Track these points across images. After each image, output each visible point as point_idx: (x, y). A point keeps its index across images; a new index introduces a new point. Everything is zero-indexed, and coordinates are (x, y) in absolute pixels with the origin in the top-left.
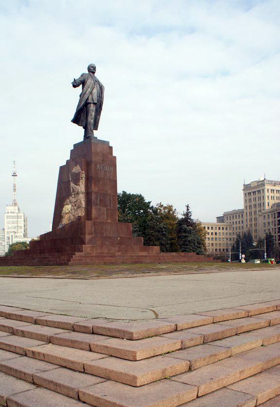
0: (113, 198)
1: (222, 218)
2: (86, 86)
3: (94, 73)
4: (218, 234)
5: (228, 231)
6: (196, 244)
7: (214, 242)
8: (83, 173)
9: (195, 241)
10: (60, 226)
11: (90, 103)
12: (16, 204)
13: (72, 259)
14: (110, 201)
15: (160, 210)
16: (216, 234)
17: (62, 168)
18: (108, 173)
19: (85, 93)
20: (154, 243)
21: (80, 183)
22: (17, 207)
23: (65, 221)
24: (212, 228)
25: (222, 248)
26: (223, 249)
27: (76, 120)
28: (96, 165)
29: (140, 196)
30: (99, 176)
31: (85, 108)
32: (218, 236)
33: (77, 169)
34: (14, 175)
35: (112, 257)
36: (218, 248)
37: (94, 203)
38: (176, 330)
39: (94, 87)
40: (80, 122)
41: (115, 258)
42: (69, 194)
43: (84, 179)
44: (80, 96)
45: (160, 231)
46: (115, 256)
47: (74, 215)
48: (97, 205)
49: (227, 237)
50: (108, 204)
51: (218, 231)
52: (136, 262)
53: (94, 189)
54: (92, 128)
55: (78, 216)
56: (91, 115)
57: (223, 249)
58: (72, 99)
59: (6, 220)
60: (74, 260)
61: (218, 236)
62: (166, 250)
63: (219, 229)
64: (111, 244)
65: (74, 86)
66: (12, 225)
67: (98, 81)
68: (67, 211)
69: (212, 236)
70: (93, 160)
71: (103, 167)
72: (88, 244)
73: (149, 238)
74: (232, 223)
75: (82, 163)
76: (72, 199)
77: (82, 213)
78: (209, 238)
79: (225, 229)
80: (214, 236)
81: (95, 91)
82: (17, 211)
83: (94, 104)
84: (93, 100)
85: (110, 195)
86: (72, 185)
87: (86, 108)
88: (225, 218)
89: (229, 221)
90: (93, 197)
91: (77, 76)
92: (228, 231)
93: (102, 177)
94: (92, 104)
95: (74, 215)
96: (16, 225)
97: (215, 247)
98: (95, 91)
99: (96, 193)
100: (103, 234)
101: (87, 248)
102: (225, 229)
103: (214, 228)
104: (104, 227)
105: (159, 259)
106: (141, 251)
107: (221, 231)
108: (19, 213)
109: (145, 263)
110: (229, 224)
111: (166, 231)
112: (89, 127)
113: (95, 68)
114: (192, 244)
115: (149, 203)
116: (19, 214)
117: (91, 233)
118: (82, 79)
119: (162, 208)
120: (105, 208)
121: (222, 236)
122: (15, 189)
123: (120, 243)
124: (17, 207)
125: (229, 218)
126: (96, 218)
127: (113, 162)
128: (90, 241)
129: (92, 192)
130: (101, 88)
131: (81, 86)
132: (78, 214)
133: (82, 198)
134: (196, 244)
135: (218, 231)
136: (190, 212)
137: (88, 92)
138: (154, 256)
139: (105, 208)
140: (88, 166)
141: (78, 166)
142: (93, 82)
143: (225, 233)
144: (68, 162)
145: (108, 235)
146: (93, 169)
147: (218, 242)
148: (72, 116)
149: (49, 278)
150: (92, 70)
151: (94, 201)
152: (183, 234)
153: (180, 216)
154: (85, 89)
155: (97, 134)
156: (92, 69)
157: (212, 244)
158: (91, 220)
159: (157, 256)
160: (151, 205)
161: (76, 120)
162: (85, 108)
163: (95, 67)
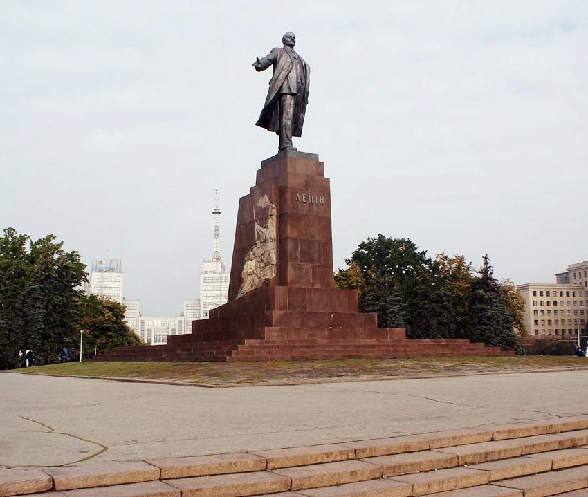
0: (324, 249)
1: (565, 275)
2: (278, 68)
3: (292, 46)
4: (558, 303)
5: (578, 298)
6: (501, 323)
7: (552, 318)
8: (273, 208)
9: (498, 317)
10: (239, 296)
11: (286, 94)
12: (218, 259)
13: (234, 351)
14: (320, 251)
15: (444, 264)
16: (555, 303)
17: (242, 200)
18: (315, 207)
19: (277, 79)
20: (427, 322)
21: (269, 224)
22: (219, 264)
23: (247, 287)
24: (541, 294)
25: (567, 328)
26: (563, 330)
27: (265, 122)
28: (294, 194)
29: (409, 242)
30: (299, 212)
31: (278, 102)
32: (558, 307)
33: (264, 201)
34: (217, 212)
35: (308, 347)
36: (560, 328)
37: (290, 257)
38: (53, 489)
39: (292, 68)
40: (271, 126)
41: (314, 349)
42: (252, 244)
43: (274, 217)
44: (270, 84)
45: (438, 300)
46: (314, 347)
47: (259, 278)
48: (296, 258)
49: (576, 308)
50: (316, 258)
51: (558, 298)
52: (350, 357)
53: (291, 232)
54: (289, 133)
55: (266, 279)
56: (287, 113)
57: (570, 331)
58: (258, 90)
59: (202, 284)
60: (238, 353)
61: (558, 307)
62: (450, 333)
63: (561, 294)
64: (318, 325)
65: (258, 69)
66: (211, 292)
67: (299, 57)
68: (249, 271)
69: (549, 308)
70: (289, 186)
71: (307, 197)
72: (276, 325)
73: (420, 313)
74: (583, 284)
75: (271, 191)
76: (257, 250)
77: (271, 274)
78: (542, 311)
79: (571, 294)
80: (552, 307)
81: (293, 75)
82: (220, 270)
83: (292, 94)
84: (289, 88)
85: (320, 244)
86: (257, 227)
87: (280, 101)
88: (571, 276)
89: (578, 280)
90: (290, 246)
91: (264, 54)
92: (578, 298)
93: (305, 212)
94: (288, 96)
95: (259, 278)
96: (219, 292)
97: (554, 327)
98: (293, 75)
99: (295, 240)
100: (305, 308)
101: (272, 333)
102: (571, 294)
103: (551, 293)
104: (307, 298)
105: (396, 351)
106: (371, 337)
107: (565, 298)
108: (222, 273)
109: (368, 358)
110: (578, 285)
111: (448, 301)
112: (284, 133)
113: (293, 39)
114: (495, 323)
115: (424, 253)
116: (223, 275)
117: (283, 308)
118: (271, 58)
119: (446, 262)
120: (311, 266)
121: (566, 307)
122: (218, 235)
123: (335, 323)
124: (219, 264)
125: (577, 275)
126: (293, 282)
127: (324, 189)
128: (280, 322)
129: (286, 238)
130: (305, 70)
131: (271, 67)
132: (266, 275)
133: (272, 248)
134: (501, 323)
135: (558, 298)
136: (490, 267)
137: (281, 77)
138: (388, 346)
139: (311, 266)
140: (281, 195)
141: (266, 196)
142: (289, 60)
143: (572, 302)
144: (252, 190)
145: (315, 311)
146: (289, 201)
147: (559, 317)
148: (257, 117)
149: (164, 383)
150: (289, 42)
151: (291, 253)
152: (478, 306)
153: (476, 275)
154: (276, 72)
155: (299, 144)
156: (289, 39)
157: (549, 321)
158: (286, 285)
159: (393, 346)
160: (427, 257)
161: (265, 122)
162: (278, 102)
163: (294, 37)
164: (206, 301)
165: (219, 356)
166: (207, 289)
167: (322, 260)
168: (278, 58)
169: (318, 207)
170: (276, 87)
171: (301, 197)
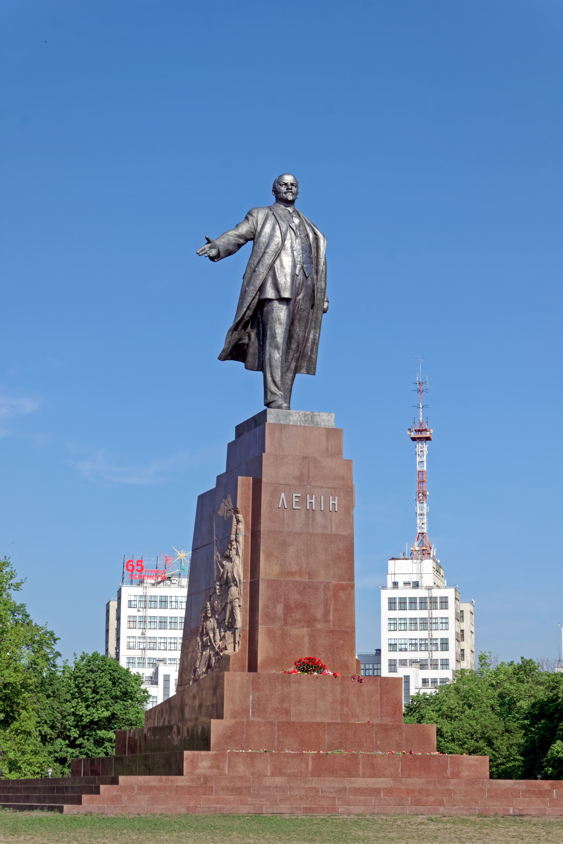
11: (270, 300)
18: (319, 519)
56: (274, 336)
59: (386, 614)
71: (303, 500)
164: (398, 656)
165: (302, 806)
166: (394, 624)
167: (331, 618)
168: (259, 229)
169: (324, 516)
170: (252, 288)
171: (290, 501)
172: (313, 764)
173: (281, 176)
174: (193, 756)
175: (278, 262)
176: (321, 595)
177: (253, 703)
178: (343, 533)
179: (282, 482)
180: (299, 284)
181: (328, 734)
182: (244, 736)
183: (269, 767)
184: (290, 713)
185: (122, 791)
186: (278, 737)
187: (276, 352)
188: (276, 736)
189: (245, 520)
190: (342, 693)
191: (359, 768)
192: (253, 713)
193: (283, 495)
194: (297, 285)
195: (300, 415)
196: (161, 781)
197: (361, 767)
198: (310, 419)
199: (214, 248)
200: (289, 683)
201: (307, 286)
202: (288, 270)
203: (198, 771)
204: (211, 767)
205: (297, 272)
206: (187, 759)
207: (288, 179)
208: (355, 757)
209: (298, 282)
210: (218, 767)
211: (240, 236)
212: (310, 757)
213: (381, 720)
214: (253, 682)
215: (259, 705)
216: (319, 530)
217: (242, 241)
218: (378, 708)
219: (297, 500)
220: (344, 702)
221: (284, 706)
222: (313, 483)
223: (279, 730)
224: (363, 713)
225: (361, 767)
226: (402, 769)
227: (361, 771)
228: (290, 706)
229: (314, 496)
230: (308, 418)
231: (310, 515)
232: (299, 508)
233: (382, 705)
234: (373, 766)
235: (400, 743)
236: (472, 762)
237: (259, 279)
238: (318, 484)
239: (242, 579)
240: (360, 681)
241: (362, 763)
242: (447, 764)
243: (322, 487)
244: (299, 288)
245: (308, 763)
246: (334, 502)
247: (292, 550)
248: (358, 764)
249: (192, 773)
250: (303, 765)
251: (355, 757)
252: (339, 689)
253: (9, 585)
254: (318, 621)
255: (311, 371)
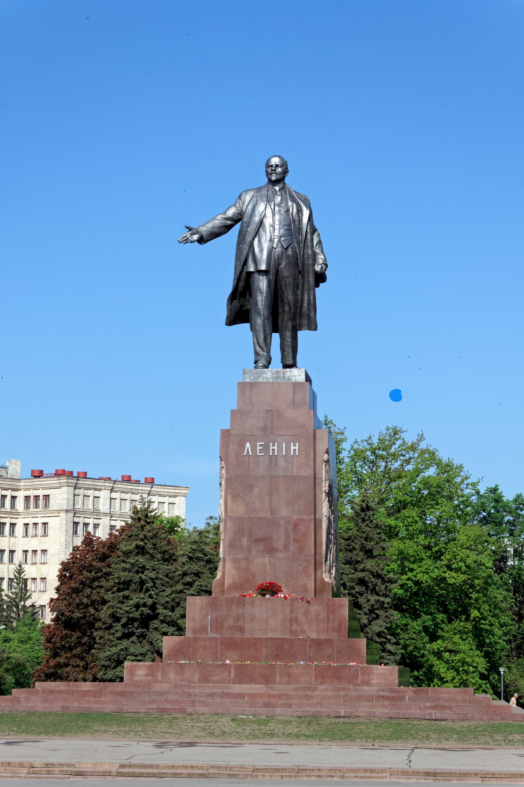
11: (253, 273)
18: (282, 463)
56: (256, 304)
71: (266, 448)
171: (254, 448)
172: (235, 673)
173: (269, 161)
174: (132, 665)
175: (256, 239)
176: (282, 528)
177: (211, 622)
178: (304, 474)
179: (248, 433)
180: (278, 256)
181: (266, 648)
182: (192, 649)
183: (196, 675)
184: (244, 630)
185: (29, 694)
186: (221, 650)
187: (259, 318)
188: (220, 649)
189: (226, 466)
190: (291, 612)
191: (276, 676)
192: (211, 629)
193: (248, 445)
194: (276, 257)
195: (272, 373)
196: (69, 686)
197: (278, 675)
198: (282, 375)
199: (195, 234)
200: (244, 605)
201: (288, 257)
202: (266, 246)
203: (136, 678)
204: (147, 675)
205: (275, 246)
206: (127, 668)
207: (275, 161)
208: (273, 667)
209: (276, 254)
210: (152, 675)
211: (227, 219)
212: (232, 667)
213: (327, 635)
214: (211, 604)
215: (217, 623)
216: (281, 473)
217: (229, 222)
218: (324, 625)
219: (261, 448)
220: (293, 620)
221: (239, 624)
222: (276, 433)
223: (221, 644)
224: (310, 629)
225: (278, 675)
226: (315, 677)
227: (278, 679)
228: (244, 624)
229: (276, 444)
230: (280, 375)
231: (273, 460)
232: (263, 454)
233: (328, 622)
234: (289, 675)
235: (331, 655)
236: (381, 672)
237: (243, 255)
238: (280, 433)
239: (223, 516)
240: (309, 602)
241: (280, 672)
242: (358, 673)
243: (284, 435)
244: (278, 259)
245: (230, 672)
246: (294, 448)
247: (256, 491)
248: (276, 673)
249: (131, 679)
250: (226, 673)
251: (273, 667)
252: (288, 609)
253: (466, 484)
254: (280, 551)
255: (313, 326)
